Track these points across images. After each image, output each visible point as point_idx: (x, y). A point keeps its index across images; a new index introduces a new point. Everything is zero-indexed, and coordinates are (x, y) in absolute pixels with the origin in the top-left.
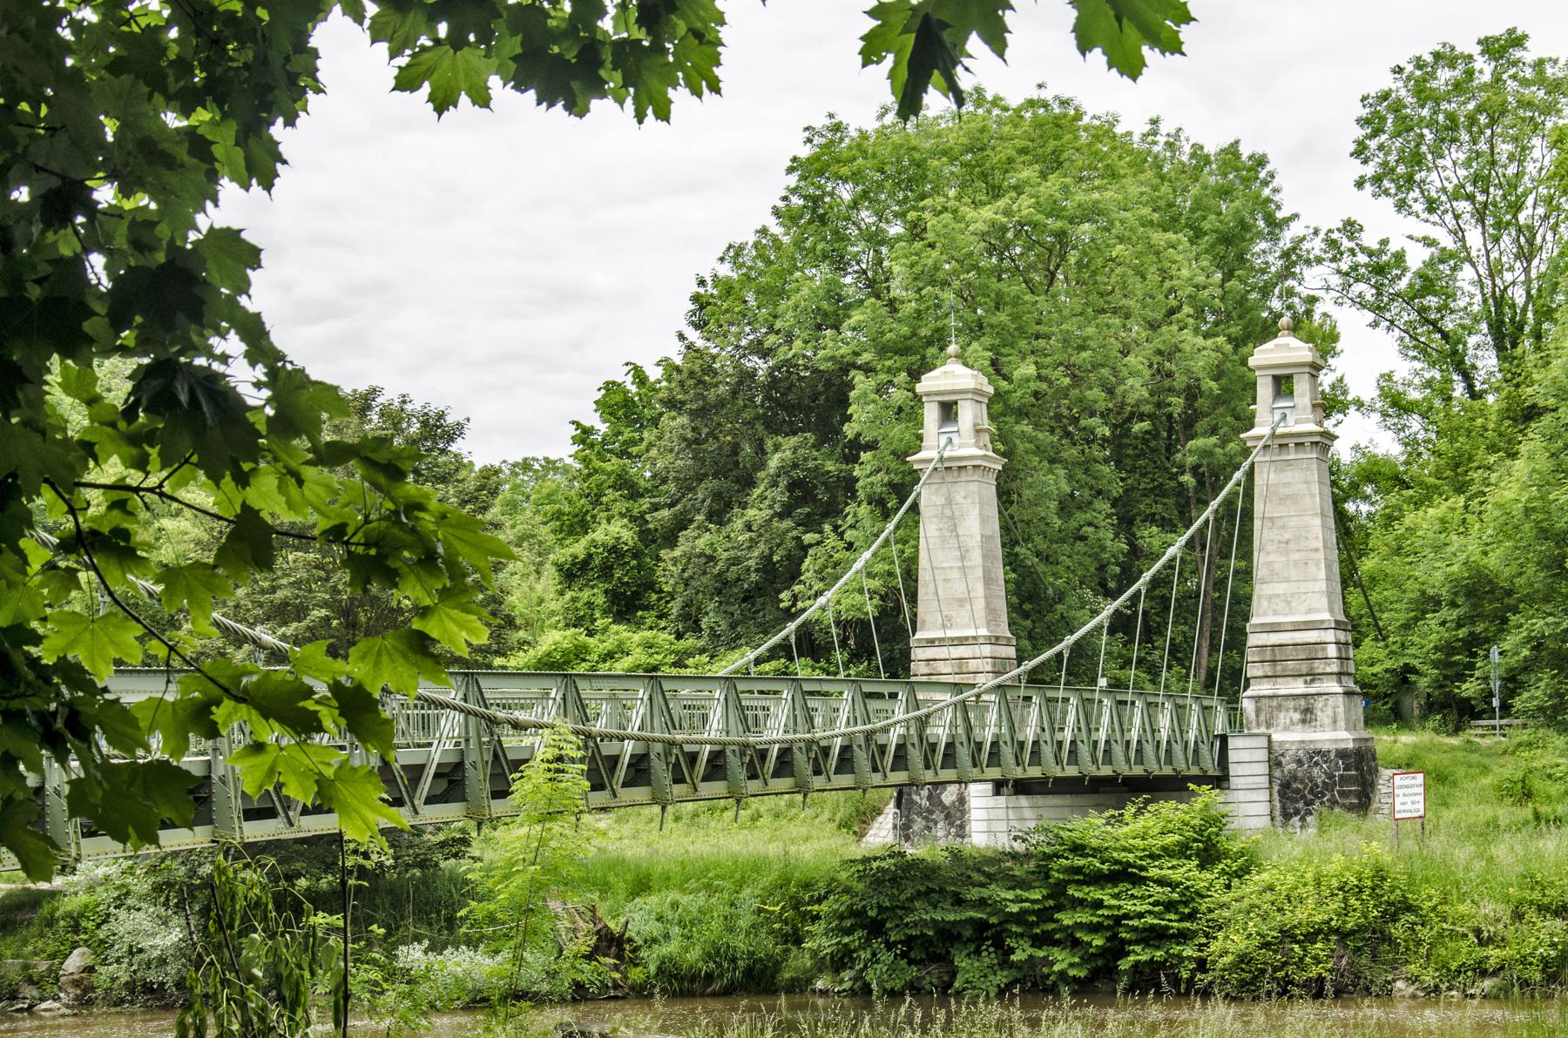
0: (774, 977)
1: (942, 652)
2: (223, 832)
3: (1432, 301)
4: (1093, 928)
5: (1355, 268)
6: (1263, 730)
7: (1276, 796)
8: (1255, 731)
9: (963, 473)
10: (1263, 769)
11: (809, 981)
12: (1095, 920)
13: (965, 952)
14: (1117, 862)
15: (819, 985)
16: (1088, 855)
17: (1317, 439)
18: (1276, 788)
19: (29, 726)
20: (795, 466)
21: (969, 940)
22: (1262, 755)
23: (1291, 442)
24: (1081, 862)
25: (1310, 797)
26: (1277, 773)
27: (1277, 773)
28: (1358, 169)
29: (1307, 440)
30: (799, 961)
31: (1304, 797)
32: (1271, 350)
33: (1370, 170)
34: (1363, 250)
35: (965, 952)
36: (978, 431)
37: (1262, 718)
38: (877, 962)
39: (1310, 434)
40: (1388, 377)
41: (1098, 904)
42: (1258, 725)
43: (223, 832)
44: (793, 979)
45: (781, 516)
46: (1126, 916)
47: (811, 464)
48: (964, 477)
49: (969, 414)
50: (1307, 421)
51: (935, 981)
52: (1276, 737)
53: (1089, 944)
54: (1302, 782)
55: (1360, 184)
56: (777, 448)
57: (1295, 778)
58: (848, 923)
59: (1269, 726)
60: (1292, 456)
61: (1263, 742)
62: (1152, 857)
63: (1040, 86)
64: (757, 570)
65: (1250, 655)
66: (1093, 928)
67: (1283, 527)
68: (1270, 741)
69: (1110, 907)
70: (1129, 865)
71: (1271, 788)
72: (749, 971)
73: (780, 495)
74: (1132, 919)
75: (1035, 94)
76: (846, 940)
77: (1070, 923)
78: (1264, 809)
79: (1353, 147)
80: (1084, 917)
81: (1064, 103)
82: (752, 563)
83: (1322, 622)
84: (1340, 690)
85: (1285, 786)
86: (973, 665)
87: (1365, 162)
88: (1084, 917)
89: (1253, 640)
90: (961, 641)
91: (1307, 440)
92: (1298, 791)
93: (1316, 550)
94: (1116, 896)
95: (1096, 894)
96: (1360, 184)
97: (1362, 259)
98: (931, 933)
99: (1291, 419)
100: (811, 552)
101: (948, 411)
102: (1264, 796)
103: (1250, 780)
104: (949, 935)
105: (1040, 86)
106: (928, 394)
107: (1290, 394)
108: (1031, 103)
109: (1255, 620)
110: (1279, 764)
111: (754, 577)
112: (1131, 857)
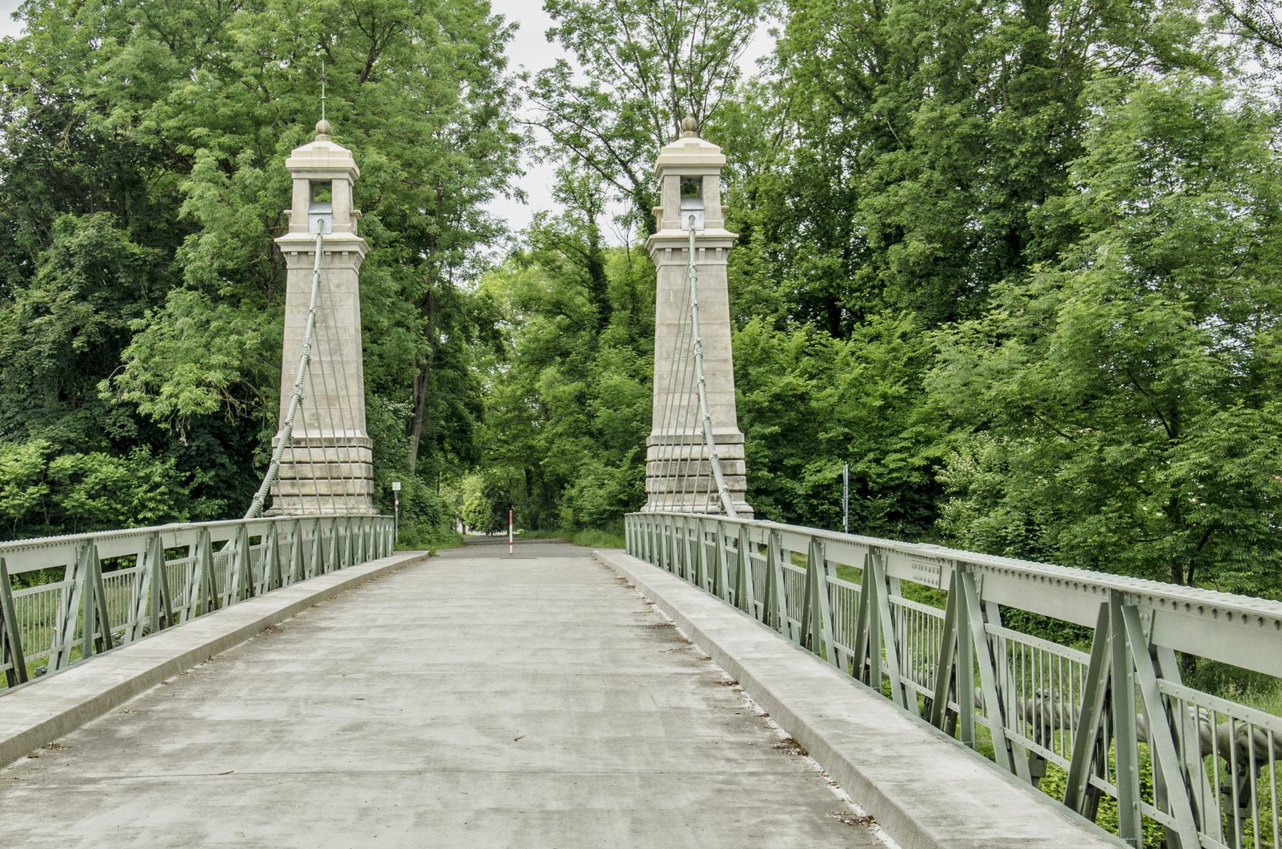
1: (317, 454)
17: (730, 245)
19: (1144, 641)
20: (99, 245)
33: (558, 24)
36: (351, 215)
39: (724, 239)
40: (543, 216)
45: (82, 297)
47: (116, 245)
48: (337, 262)
49: (342, 195)
50: (342, 230)
56: (69, 229)
64: (51, 356)
65: (650, 470)
73: (76, 276)
82: (45, 348)
83: (732, 436)
84: (751, 509)
86: (345, 469)
87: (553, 17)
89: (651, 454)
90: (331, 443)
93: (725, 361)
97: (570, 98)
99: (699, 223)
100: (135, 338)
101: (320, 189)
106: (298, 171)
107: (327, 202)
109: (656, 432)
111: (47, 364)
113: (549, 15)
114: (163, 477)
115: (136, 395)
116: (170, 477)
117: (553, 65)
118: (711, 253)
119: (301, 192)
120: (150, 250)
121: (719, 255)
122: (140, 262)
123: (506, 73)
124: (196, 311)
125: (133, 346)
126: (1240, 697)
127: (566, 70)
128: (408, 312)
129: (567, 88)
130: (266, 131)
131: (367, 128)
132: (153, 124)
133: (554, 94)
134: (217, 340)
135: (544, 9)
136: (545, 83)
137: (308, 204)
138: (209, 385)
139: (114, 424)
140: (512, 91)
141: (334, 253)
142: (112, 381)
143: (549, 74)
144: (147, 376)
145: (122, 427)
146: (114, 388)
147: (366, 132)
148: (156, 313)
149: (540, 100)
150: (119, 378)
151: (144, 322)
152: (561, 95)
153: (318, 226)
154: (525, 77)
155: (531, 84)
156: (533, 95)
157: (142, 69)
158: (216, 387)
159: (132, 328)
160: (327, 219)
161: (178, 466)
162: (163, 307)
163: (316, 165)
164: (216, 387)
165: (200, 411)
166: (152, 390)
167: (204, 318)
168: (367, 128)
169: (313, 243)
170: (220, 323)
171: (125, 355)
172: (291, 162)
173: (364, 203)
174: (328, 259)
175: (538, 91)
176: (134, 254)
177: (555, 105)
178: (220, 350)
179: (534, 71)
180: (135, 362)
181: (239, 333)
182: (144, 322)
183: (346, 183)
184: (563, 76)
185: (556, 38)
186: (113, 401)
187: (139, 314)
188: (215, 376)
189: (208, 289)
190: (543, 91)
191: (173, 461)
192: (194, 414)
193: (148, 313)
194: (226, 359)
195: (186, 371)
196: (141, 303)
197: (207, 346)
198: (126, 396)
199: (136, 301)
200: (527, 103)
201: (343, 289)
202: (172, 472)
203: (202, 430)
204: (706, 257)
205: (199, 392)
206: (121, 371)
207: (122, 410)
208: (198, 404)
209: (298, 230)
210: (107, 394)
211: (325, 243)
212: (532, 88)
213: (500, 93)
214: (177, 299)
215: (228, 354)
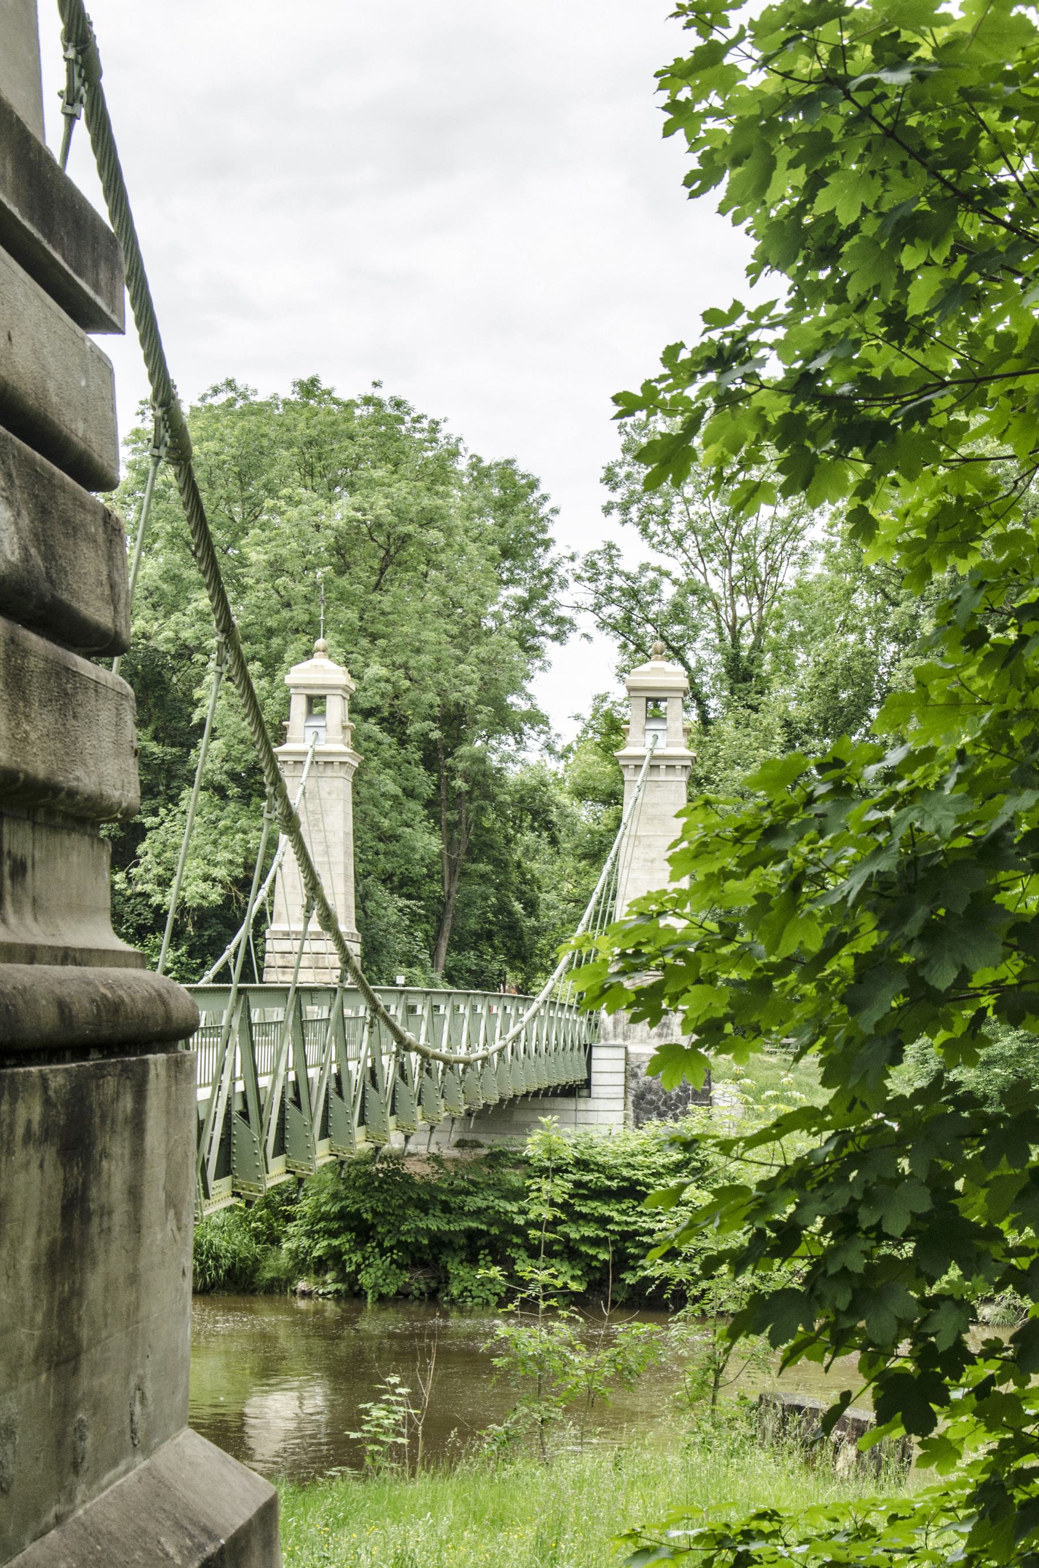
0: (252, 1276)
2: (297, 1162)
3: (677, 629)
4: (596, 1242)
5: (610, 589)
6: (620, 1041)
7: (630, 1106)
8: (612, 1042)
9: (329, 768)
10: (620, 1079)
11: (289, 1281)
12: (602, 1234)
13: (457, 1260)
14: (624, 1179)
15: (302, 1285)
16: (592, 1170)
17: (689, 763)
18: (631, 1098)
21: (462, 1248)
22: (621, 1066)
23: (663, 764)
24: (587, 1177)
25: (663, 1108)
26: (633, 1084)
27: (633, 1084)
28: (606, 495)
29: (678, 763)
30: (281, 1258)
31: (657, 1108)
32: (648, 673)
33: (617, 497)
34: (621, 573)
35: (457, 1260)
36: (344, 728)
37: (620, 1030)
38: (370, 1265)
39: (683, 758)
40: (604, 698)
41: (603, 1221)
42: (615, 1036)
43: (297, 1162)
44: (273, 1279)
46: (636, 1233)
48: (329, 772)
49: (336, 709)
50: (335, 742)
51: (423, 1287)
52: (632, 1049)
53: (595, 1258)
54: (656, 1093)
55: (607, 510)
57: (650, 1090)
58: (335, 1225)
59: (626, 1037)
60: (662, 778)
61: (621, 1054)
62: (657, 1175)
63: (376, 384)
66: (596, 1242)
67: (649, 846)
68: (627, 1053)
69: (618, 1223)
70: (638, 1182)
71: (626, 1098)
72: (229, 1272)
74: (643, 1235)
75: (370, 391)
76: (335, 1242)
77: (577, 1236)
78: (619, 1117)
79: (602, 474)
80: (589, 1231)
81: (398, 404)
85: (640, 1097)
87: (613, 489)
88: (589, 1231)
91: (678, 763)
92: (651, 1102)
94: (623, 1212)
95: (604, 1210)
96: (607, 510)
97: (618, 581)
98: (425, 1242)
99: (662, 742)
100: (149, 834)
101: (315, 703)
102: (619, 1105)
103: (609, 1089)
104: (440, 1243)
105: (376, 384)
106: (296, 687)
107: (323, 714)
108: (368, 401)
110: (635, 1076)
112: (639, 1175)
113: (607, 487)
114: (175, 964)
115: (148, 888)
116: (182, 964)
117: (601, 547)
118: (671, 770)
119: (298, 706)
120: (169, 750)
121: (678, 772)
122: (158, 761)
123: (554, 553)
124: (206, 810)
125: (148, 841)
126: (102, 964)
127: (614, 552)
128: (415, 813)
129: (616, 571)
130: (276, 642)
131: (374, 637)
132: (171, 634)
133: (601, 577)
134: (224, 838)
135: (602, 481)
136: (593, 565)
137: (304, 717)
138: (214, 880)
139: (132, 912)
140: (561, 571)
141: (323, 762)
142: (128, 873)
143: (596, 556)
144: (160, 870)
145: (140, 915)
146: (129, 880)
147: (372, 642)
148: (170, 811)
149: (587, 583)
150: (134, 871)
151: (157, 820)
152: (610, 578)
153: (313, 737)
154: (572, 559)
155: (578, 565)
156: (578, 578)
157: (165, 581)
158: (221, 882)
159: (147, 826)
160: (321, 731)
161: (190, 954)
162: (176, 805)
163: (312, 682)
164: (221, 882)
165: (205, 904)
166: (163, 883)
167: (213, 817)
168: (374, 637)
169: (305, 754)
170: (227, 822)
171: (140, 850)
172: (289, 680)
173: (359, 711)
174: (321, 768)
175: (585, 575)
176: (154, 753)
177: (602, 588)
178: (226, 847)
179: (583, 552)
180: (149, 857)
181: (245, 832)
182: (157, 820)
183: (339, 698)
184: (611, 560)
185: (615, 512)
186: (129, 892)
187: (155, 813)
188: (220, 872)
189: (220, 790)
190: (588, 575)
191: (184, 949)
192: (200, 908)
193: (162, 811)
194: (230, 857)
195: (195, 867)
196: (160, 800)
197: (215, 843)
198: (139, 888)
199: (155, 797)
200: (573, 585)
201: (334, 796)
202: (184, 959)
203: (214, 921)
204: (667, 774)
205: (204, 887)
206: (136, 865)
207: (139, 900)
208: (203, 897)
209: (294, 741)
210: (125, 886)
211: (316, 754)
212: (578, 571)
213: (548, 572)
214: (191, 797)
215: (234, 852)
